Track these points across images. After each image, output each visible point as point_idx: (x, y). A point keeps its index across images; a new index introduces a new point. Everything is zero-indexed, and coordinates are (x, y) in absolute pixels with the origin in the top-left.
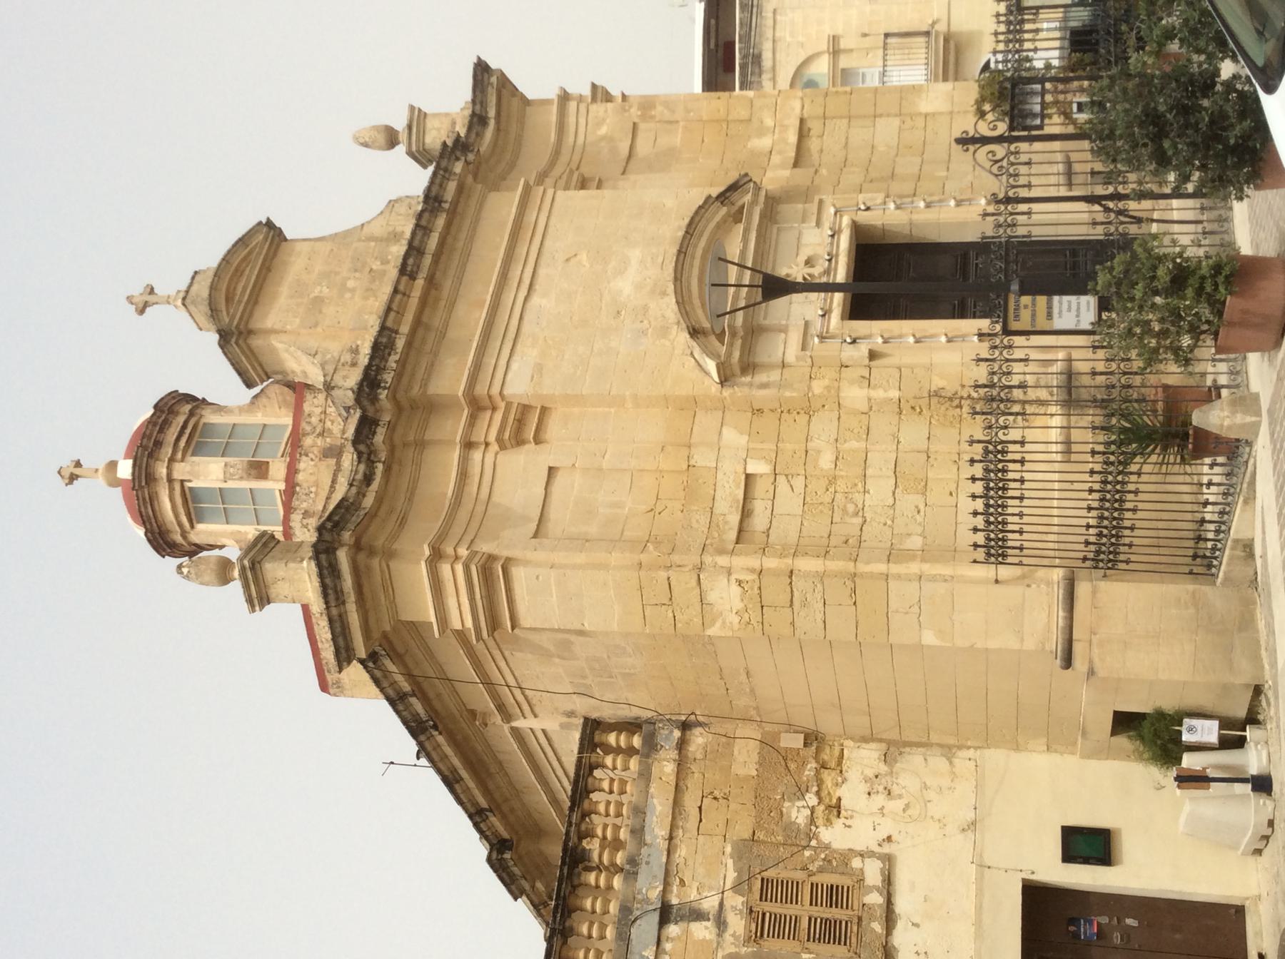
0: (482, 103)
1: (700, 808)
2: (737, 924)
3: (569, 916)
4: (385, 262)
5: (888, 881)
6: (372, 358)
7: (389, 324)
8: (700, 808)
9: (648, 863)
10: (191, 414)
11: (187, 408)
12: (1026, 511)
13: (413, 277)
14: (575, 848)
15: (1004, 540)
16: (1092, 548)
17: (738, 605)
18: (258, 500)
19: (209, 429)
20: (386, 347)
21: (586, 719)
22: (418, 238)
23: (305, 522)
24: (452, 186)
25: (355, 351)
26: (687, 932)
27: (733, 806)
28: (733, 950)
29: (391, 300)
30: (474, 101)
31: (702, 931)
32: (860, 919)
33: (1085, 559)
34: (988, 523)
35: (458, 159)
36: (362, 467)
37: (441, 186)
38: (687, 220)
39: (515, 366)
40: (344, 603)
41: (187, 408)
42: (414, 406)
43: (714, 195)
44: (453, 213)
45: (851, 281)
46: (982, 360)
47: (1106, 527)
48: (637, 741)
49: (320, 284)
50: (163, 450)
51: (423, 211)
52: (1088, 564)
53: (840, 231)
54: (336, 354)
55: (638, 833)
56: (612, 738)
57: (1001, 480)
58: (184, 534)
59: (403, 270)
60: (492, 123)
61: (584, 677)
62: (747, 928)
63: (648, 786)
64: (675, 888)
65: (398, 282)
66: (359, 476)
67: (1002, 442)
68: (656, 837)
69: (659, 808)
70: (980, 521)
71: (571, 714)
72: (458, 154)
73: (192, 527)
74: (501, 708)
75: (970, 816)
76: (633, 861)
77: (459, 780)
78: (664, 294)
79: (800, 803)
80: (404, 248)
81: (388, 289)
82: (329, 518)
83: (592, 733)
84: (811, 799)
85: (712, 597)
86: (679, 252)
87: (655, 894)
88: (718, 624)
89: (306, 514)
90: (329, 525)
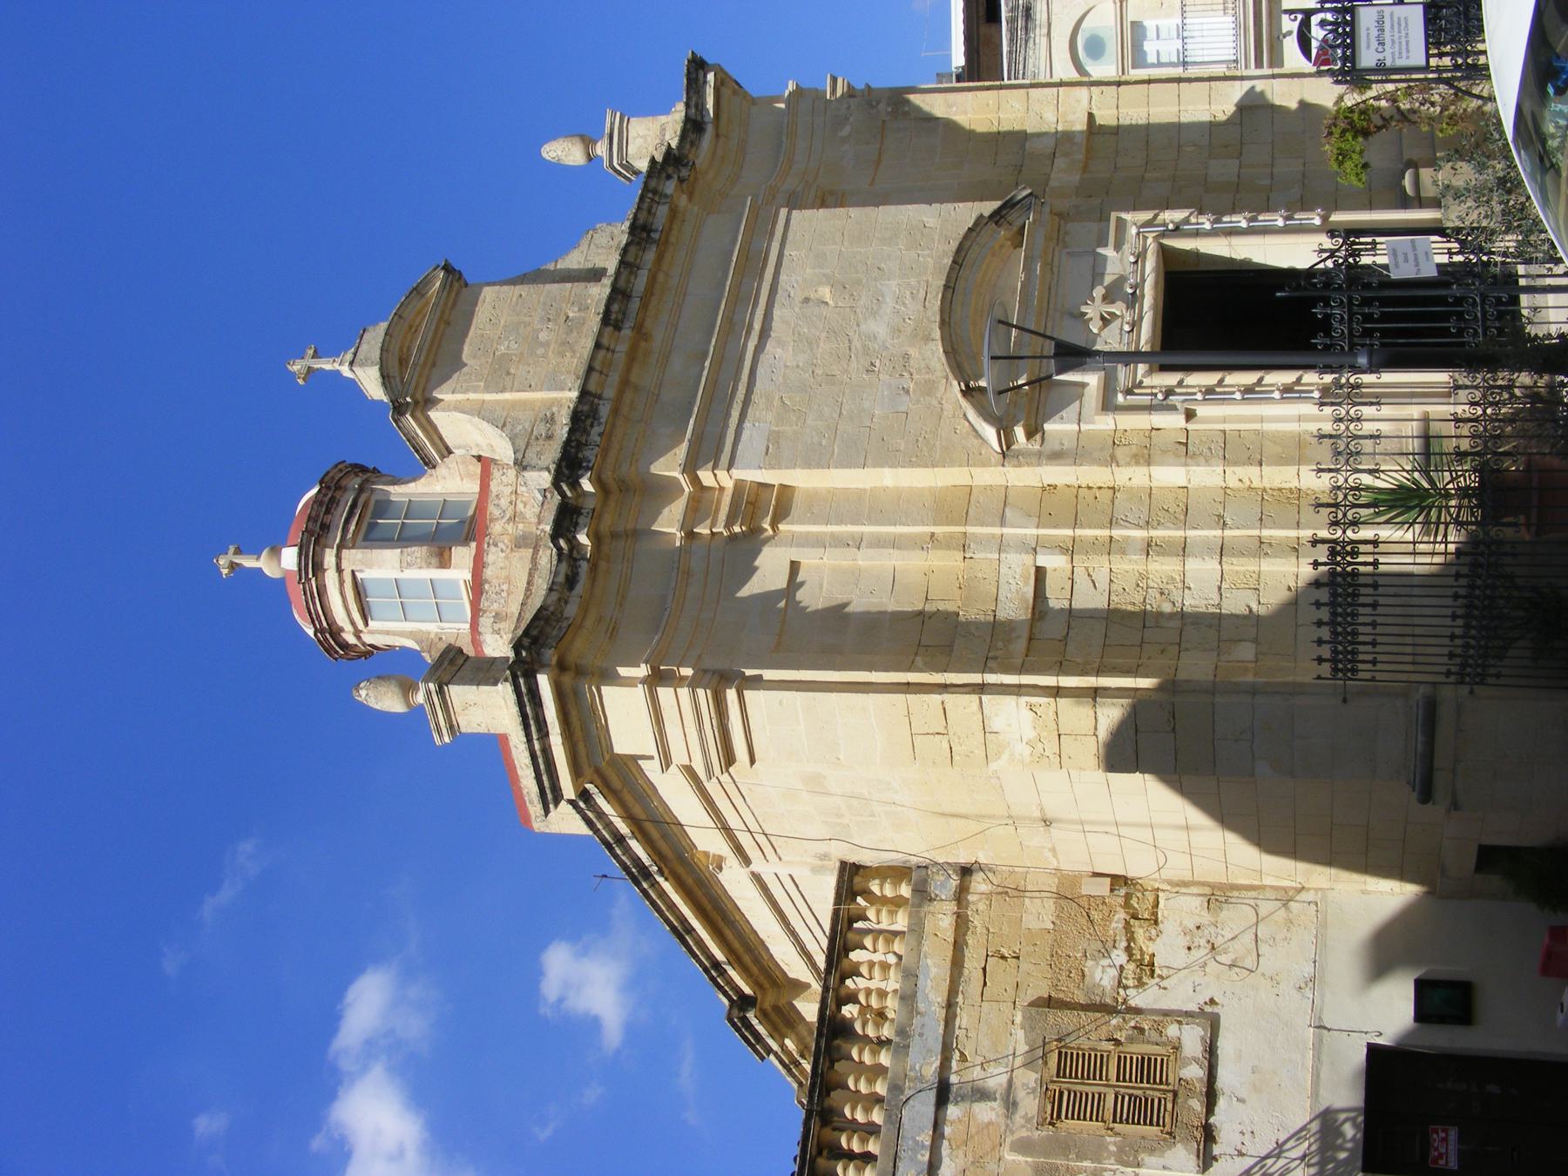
0: (696, 106)
1: (984, 969)
2: (1029, 1105)
3: (828, 1095)
5: (1211, 1051)
6: (571, 432)
7: (592, 387)
8: (984, 969)
9: (921, 1035)
10: (361, 490)
11: (355, 483)
12: (1379, 620)
13: (618, 328)
14: (833, 1018)
15: (1353, 653)
16: (1458, 660)
17: (1029, 734)
18: (439, 594)
19: (384, 507)
20: (587, 417)
21: (843, 864)
22: (623, 278)
23: (496, 627)
24: (662, 211)
25: (551, 420)
26: (969, 1114)
27: (1024, 966)
28: (1024, 1133)
29: (593, 358)
31: (987, 1112)
32: (1175, 1094)
33: (1448, 673)
34: (1335, 633)
35: (669, 177)
36: (564, 567)
37: (649, 212)
38: (954, 245)
40: (547, 734)
41: (355, 483)
42: (625, 487)
43: (986, 214)
44: (663, 245)
45: (1158, 349)
47: (1473, 637)
48: (905, 890)
49: (507, 338)
50: (331, 535)
51: (627, 245)
52: (1452, 679)
54: (527, 425)
55: (908, 998)
56: (875, 887)
57: (1350, 585)
58: (357, 634)
59: (606, 320)
60: (710, 129)
61: (841, 816)
62: (1042, 1110)
63: (920, 943)
64: (954, 1064)
65: (600, 334)
66: (561, 578)
67: (1352, 542)
68: (931, 1004)
69: (934, 971)
70: (1325, 633)
71: (825, 857)
72: (670, 170)
73: (366, 624)
74: (739, 850)
75: (1309, 970)
76: (902, 1032)
77: (690, 930)
78: (928, 339)
79: (1106, 962)
80: (608, 291)
81: (589, 344)
82: (526, 633)
83: (851, 880)
84: (1120, 957)
85: (996, 724)
86: (946, 287)
87: (931, 1070)
88: (1005, 757)
89: (498, 617)
90: (526, 642)
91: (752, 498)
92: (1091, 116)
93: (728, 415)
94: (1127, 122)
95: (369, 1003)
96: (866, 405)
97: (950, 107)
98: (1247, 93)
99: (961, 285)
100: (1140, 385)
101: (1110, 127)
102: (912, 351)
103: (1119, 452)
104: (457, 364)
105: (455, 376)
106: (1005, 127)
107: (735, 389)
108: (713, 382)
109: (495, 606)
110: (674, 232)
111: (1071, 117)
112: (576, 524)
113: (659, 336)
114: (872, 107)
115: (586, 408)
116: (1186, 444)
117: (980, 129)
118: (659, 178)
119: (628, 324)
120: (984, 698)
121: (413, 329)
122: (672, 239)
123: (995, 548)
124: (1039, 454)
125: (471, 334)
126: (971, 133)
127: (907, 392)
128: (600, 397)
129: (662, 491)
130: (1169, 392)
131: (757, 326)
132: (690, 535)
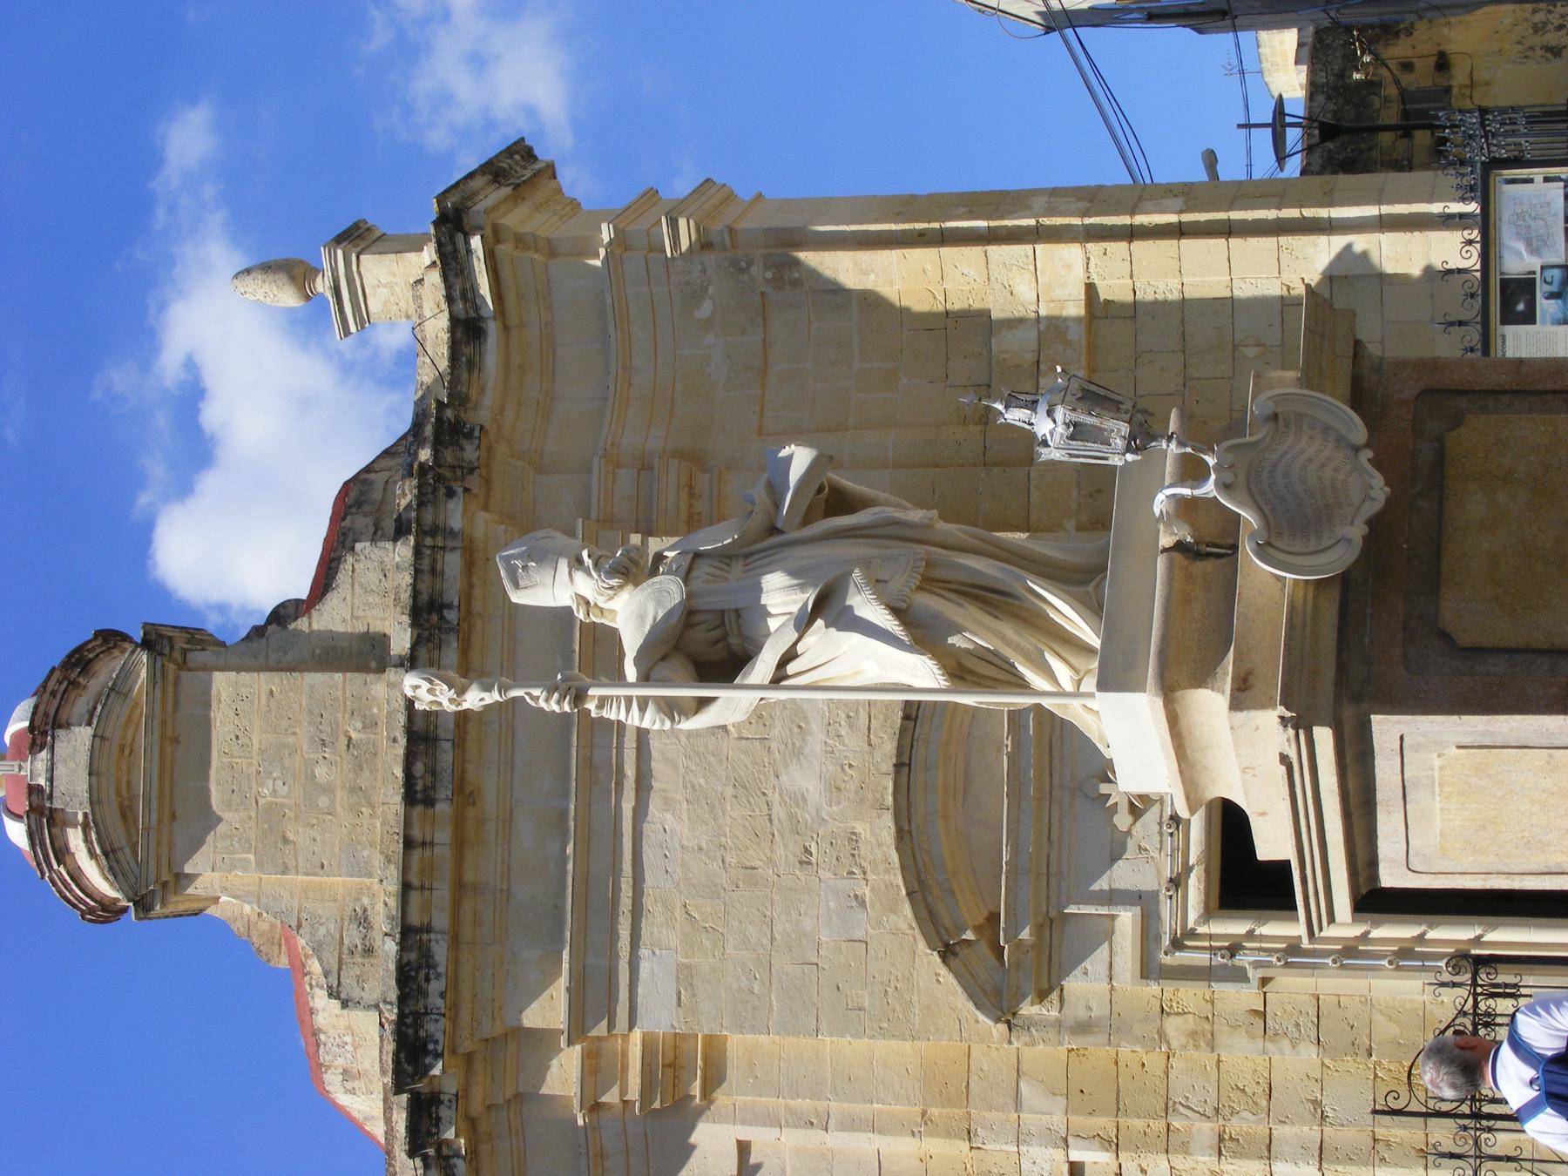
4: (370, 725)
7: (415, 919)
13: (430, 802)
23: (349, 1085)
24: (452, 563)
25: (363, 920)
30: (449, 299)
37: (433, 571)
39: (645, 968)
46: (1451, 324)
53: (1188, 869)
59: (410, 797)
60: (492, 328)
91: (670, 1058)
92: (1090, 289)
93: (614, 935)
94: (1150, 297)
95: (189, 138)
96: (807, 923)
97: (865, 273)
98: (1339, 257)
99: (920, 753)
100: (1192, 934)
101: (1122, 305)
102: (859, 828)
103: (1172, 1025)
104: (209, 820)
105: (210, 838)
106: (956, 305)
107: (617, 889)
108: (585, 880)
109: (340, 1061)
110: (477, 592)
111: (1058, 294)
112: (438, 1119)
113: (490, 798)
114: (742, 271)
115: (413, 956)
116: (1263, 1015)
117: (919, 305)
118: (435, 502)
119: (443, 793)
120: (1039, 247)
121: (126, 750)
122: (477, 606)
123: (1012, 1137)
124: (1059, 1025)
125: (214, 763)
126: (904, 311)
127: (862, 903)
128: (428, 929)
129: (541, 1043)
130: (1234, 949)
131: (630, 770)
132: (595, 1108)
